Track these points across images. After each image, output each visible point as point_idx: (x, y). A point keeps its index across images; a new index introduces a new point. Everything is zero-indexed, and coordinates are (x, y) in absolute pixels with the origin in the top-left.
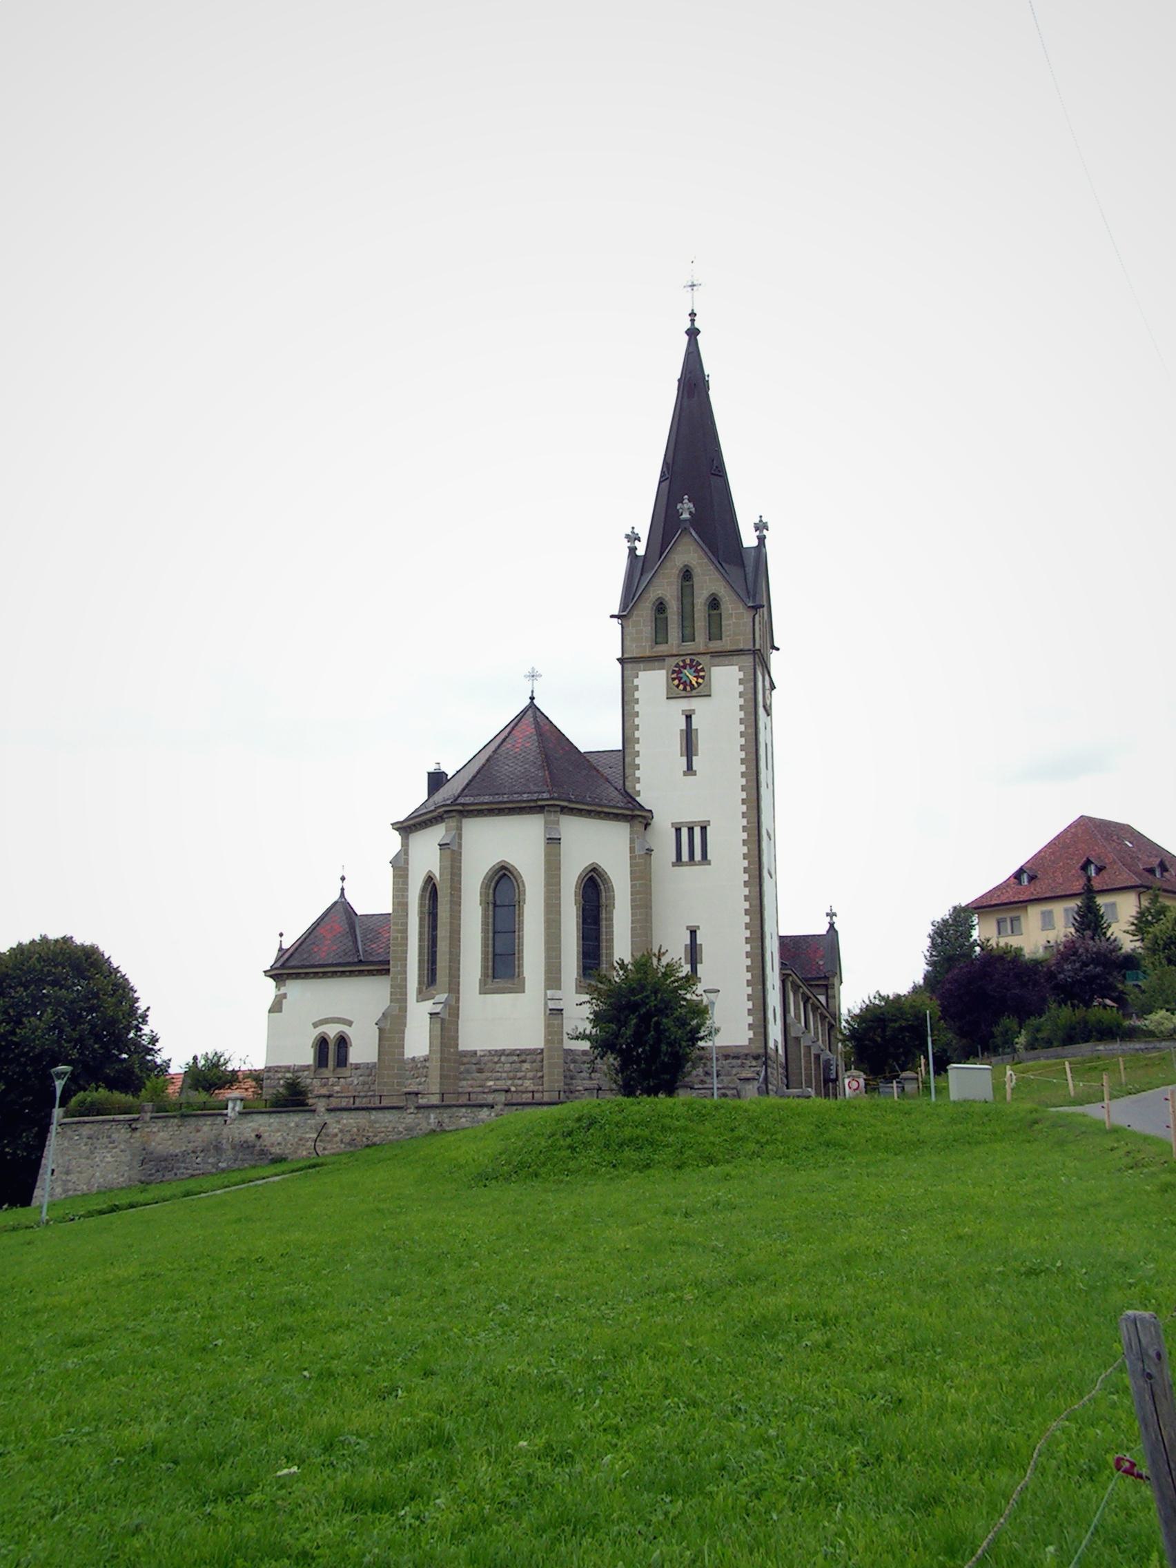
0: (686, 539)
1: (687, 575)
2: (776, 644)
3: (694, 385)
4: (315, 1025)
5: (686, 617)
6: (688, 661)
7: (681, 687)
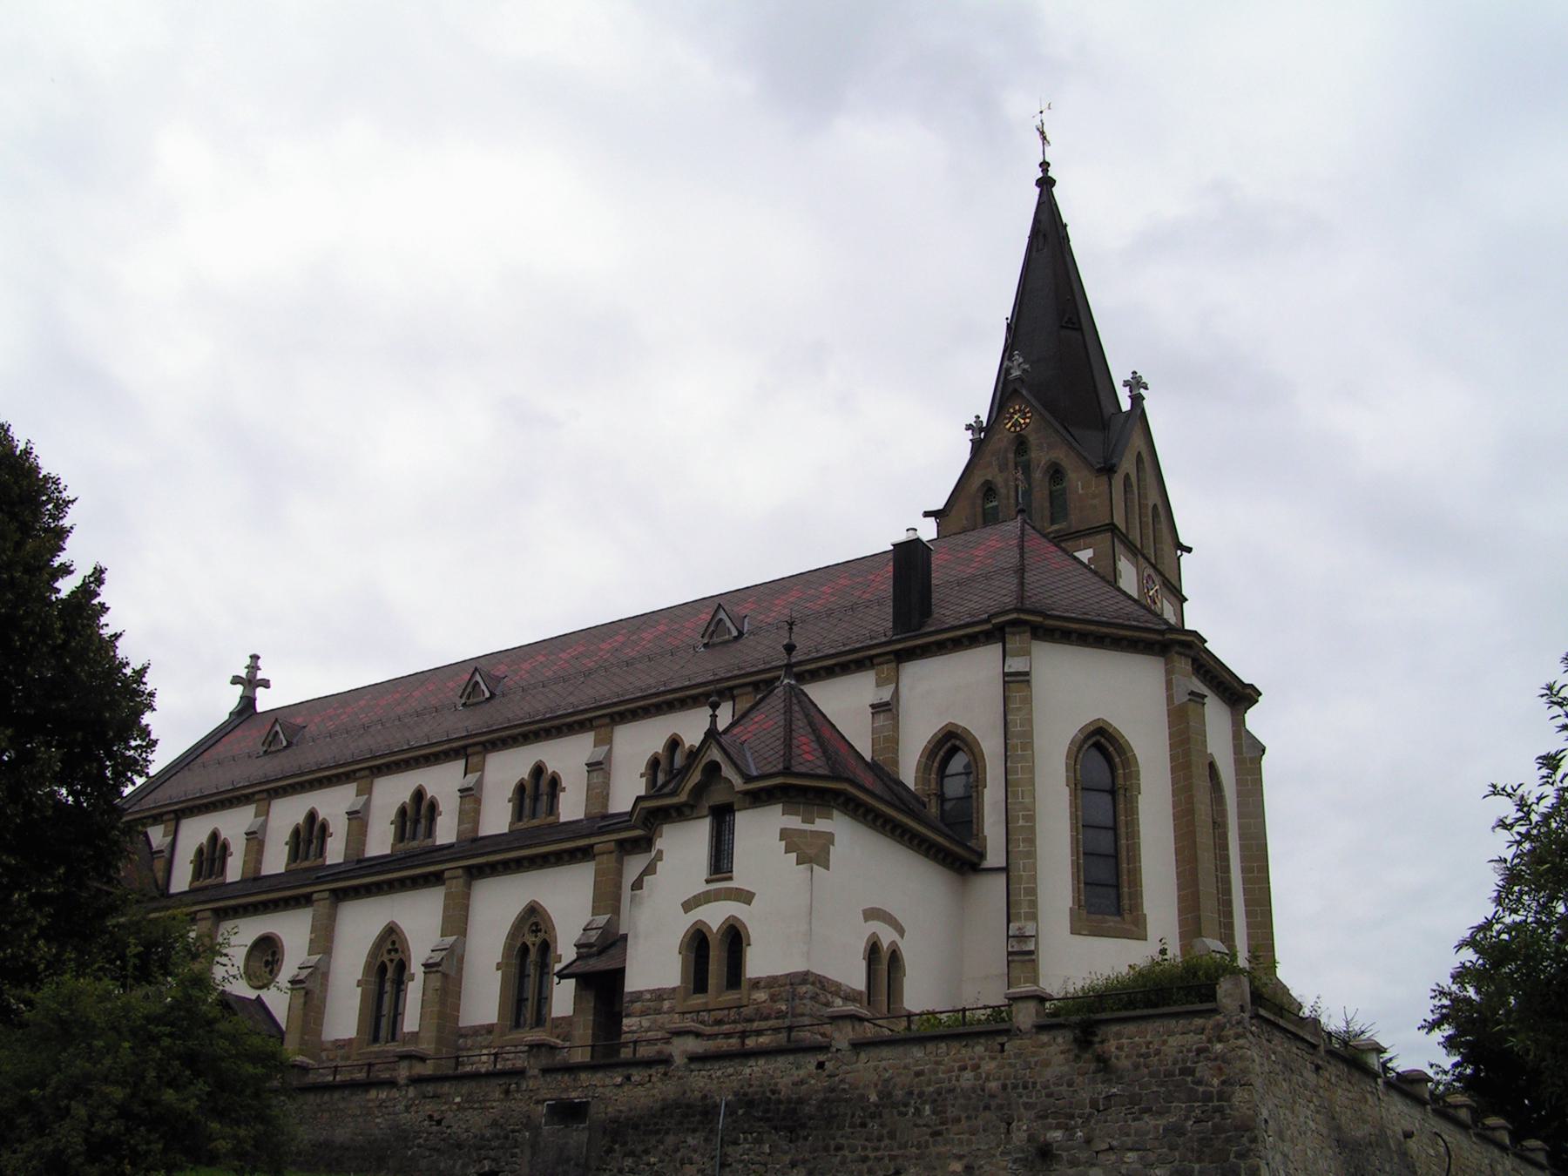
3: (1049, 236)
4: (688, 906)
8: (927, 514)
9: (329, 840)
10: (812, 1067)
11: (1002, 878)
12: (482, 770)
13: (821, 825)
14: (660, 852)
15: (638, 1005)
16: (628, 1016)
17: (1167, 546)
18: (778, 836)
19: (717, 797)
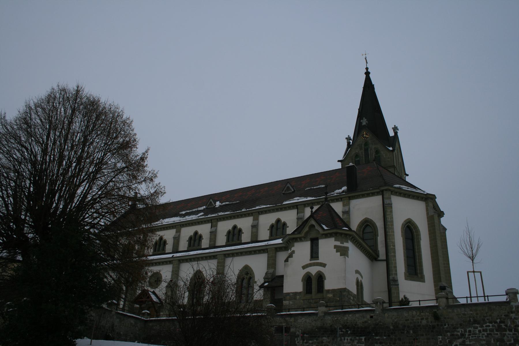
2: (407, 173)
3: (369, 88)
8: (339, 161)
9: (167, 245)
10: (368, 317)
11: (385, 263)
12: (217, 226)
13: (345, 245)
14: (293, 252)
15: (288, 297)
16: (285, 300)
17: (403, 174)
18: (333, 247)
19: (313, 235)
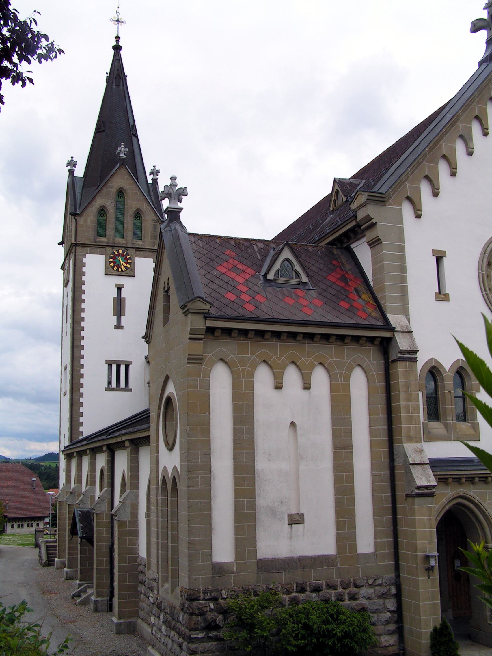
0: (123, 171)
1: (121, 193)
5: (120, 221)
6: (121, 252)
7: (115, 268)
